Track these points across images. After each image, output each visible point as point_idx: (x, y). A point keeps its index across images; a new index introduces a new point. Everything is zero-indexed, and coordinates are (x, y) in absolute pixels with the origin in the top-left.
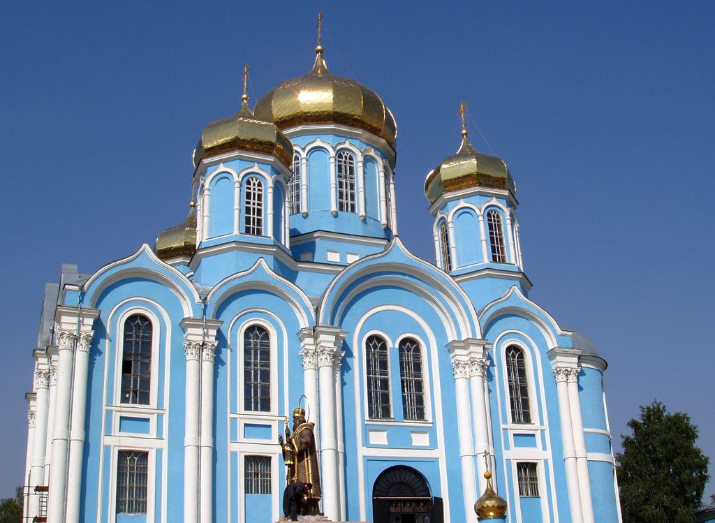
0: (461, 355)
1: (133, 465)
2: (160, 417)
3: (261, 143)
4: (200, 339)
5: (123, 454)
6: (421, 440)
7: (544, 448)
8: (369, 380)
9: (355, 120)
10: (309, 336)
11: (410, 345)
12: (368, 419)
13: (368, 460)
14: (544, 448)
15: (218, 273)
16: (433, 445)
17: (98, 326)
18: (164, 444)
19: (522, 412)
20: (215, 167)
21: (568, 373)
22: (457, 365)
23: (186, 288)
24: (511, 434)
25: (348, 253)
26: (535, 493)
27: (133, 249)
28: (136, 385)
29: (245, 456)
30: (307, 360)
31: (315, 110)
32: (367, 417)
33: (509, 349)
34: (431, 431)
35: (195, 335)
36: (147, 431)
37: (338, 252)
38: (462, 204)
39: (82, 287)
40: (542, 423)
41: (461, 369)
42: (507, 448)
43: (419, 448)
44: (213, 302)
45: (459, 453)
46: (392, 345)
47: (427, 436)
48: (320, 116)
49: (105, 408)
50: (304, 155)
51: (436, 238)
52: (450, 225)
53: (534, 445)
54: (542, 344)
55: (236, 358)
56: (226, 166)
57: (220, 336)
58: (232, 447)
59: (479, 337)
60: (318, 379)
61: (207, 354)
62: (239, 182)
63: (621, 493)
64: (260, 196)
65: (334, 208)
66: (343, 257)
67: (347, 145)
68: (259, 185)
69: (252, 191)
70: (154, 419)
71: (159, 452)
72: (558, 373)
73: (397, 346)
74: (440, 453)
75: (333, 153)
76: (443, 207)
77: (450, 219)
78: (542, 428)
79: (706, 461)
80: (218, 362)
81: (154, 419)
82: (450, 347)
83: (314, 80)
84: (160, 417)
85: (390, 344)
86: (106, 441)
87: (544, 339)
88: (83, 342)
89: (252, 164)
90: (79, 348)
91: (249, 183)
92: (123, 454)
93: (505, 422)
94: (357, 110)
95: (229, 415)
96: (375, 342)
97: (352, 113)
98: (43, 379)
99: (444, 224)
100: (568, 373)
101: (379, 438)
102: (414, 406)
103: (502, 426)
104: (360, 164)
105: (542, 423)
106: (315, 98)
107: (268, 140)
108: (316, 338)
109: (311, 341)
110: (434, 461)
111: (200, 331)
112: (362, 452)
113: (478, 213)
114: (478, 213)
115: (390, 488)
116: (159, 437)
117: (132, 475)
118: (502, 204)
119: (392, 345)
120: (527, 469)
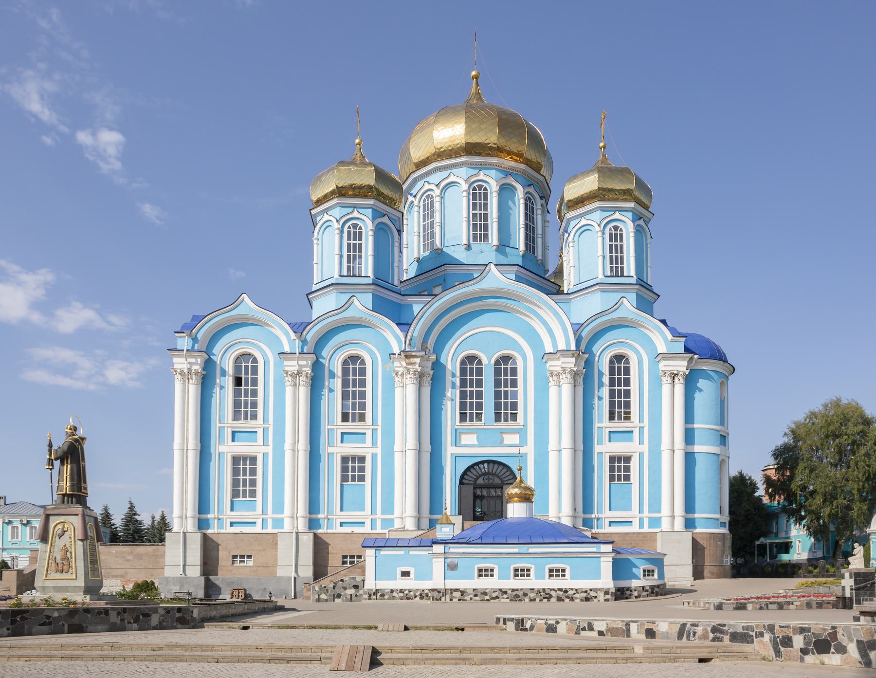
0: (556, 365)
2: (265, 430)
3: (361, 187)
4: (295, 369)
5: (345, 459)
7: (641, 442)
9: (491, 148)
13: (456, 457)
14: (641, 442)
15: (587, 307)
16: (523, 442)
17: (209, 364)
18: (269, 450)
21: (674, 376)
27: (235, 302)
28: (620, 409)
30: (396, 379)
31: (447, 145)
32: (458, 423)
34: (522, 432)
43: (506, 445)
46: (488, 362)
48: (453, 149)
50: (437, 192)
53: (631, 440)
58: (222, 449)
59: (573, 348)
61: (303, 381)
62: (338, 229)
63: (171, 466)
67: (481, 176)
70: (260, 432)
73: (493, 362)
74: (529, 449)
75: (465, 186)
78: (641, 425)
81: (260, 432)
82: (545, 356)
83: (445, 112)
84: (265, 430)
85: (485, 361)
86: (222, 449)
92: (345, 459)
94: (492, 138)
97: (487, 142)
102: (505, 410)
106: (451, 132)
107: (367, 183)
112: (449, 450)
115: (480, 476)
116: (265, 444)
119: (488, 362)
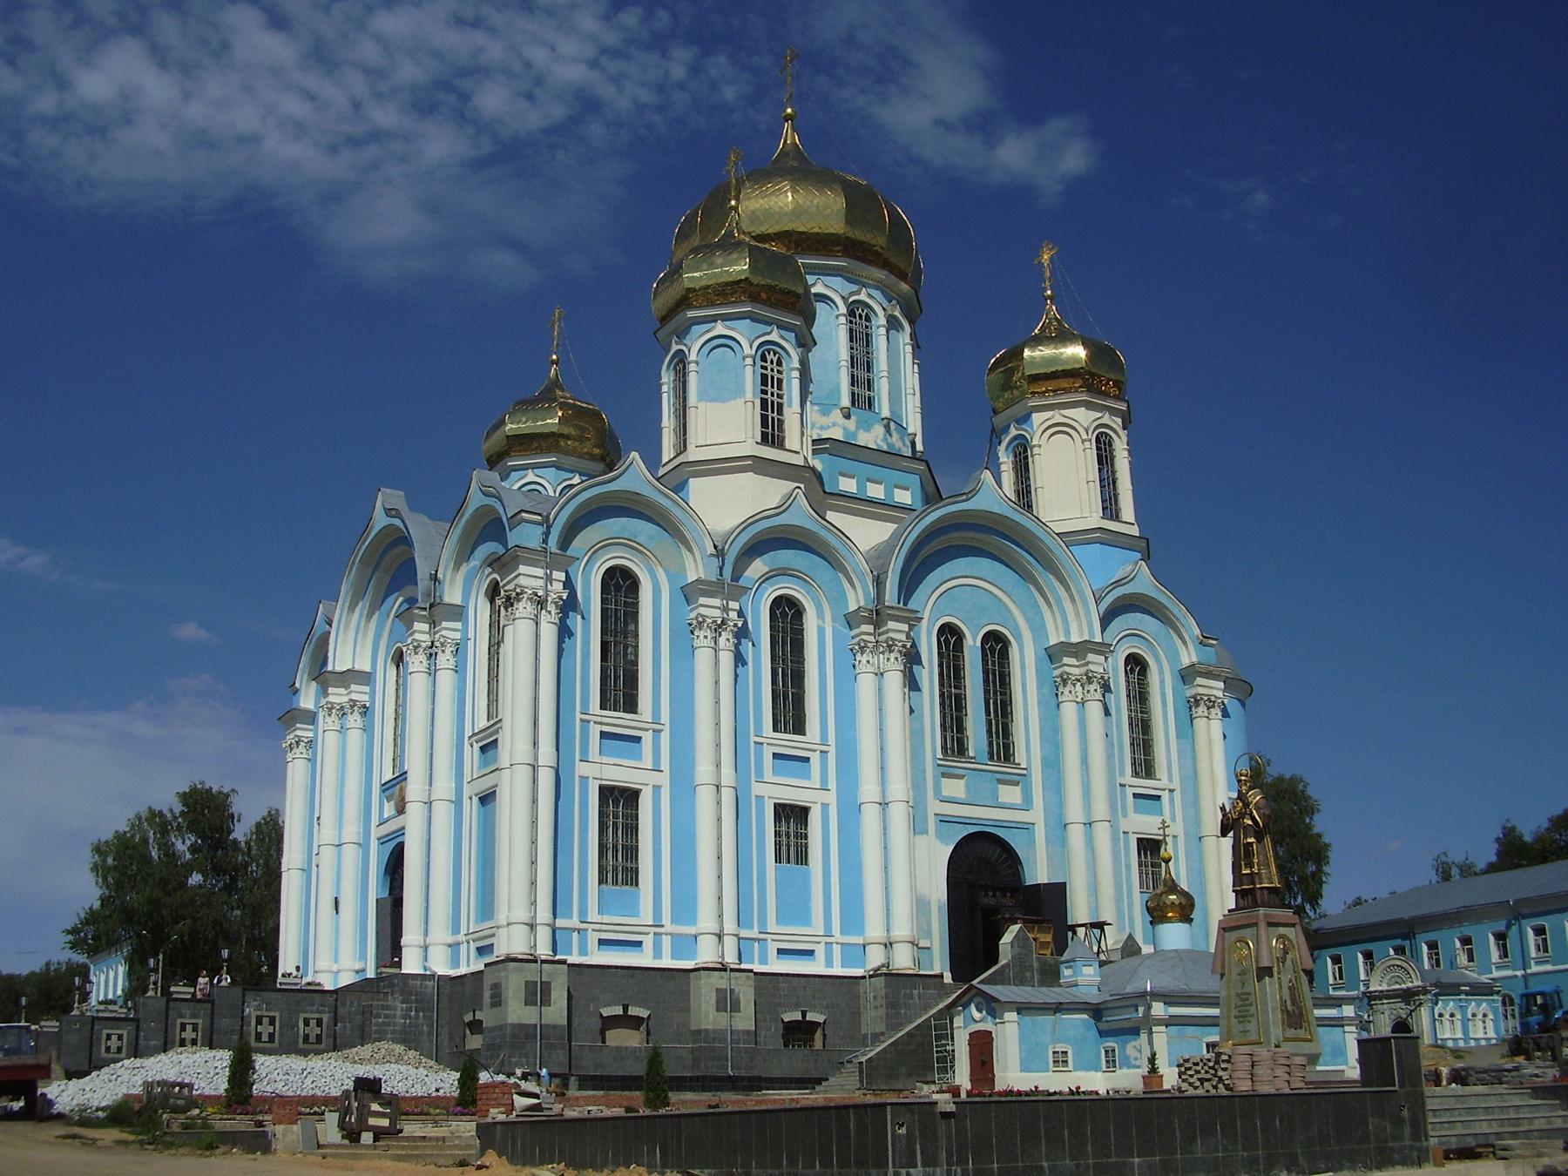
1: (620, 803)
6: (1009, 794)
8: (942, 695)
10: (869, 621)
11: (996, 646)
12: (598, 711)
16: (1027, 805)
19: (620, 688)
20: (708, 326)
22: (700, 623)
23: (1085, 604)
24: (768, 752)
25: (897, 487)
26: (802, 857)
29: (601, 787)
33: (611, 572)
35: (710, 608)
36: (638, 756)
37: (879, 483)
38: (720, 329)
39: (548, 517)
40: (1170, 780)
41: (1069, 687)
42: (1125, 816)
44: (732, 554)
45: (692, 777)
47: (1018, 789)
49: (578, 716)
51: (665, 388)
52: (692, 367)
54: (1173, 657)
55: (929, 674)
56: (727, 327)
57: (568, 584)
60: (537, 636)
64: (780, 381)
65: (846, 401)
66: (861, 487)
67: (863, 297)
68: (779, 363)
69: (769, 372)
71: (825, 806)
72: (1197, 703)
74: (1036, 815)
75: (843, 309)
76: (682, 333)
77: (693, 357)
79: (1327, 846)
80: (564, 632)
87: (1175, 650)
88: (552, 608)
89: (769, 329)
90: (722, 640)
91: (764, 359)
93: (1122, 774)
95: (754, 739)
96: (950, 637)
98: (422, 657)
99: (681, 361)
100: (720, 627)
101: (954, 788)
103: (754, 739)
104: (883, 331)
105: (1170, 780)
108: (877, 626)
109: (870, 628)
110: (1027, 827)
111: (717, 602)
113: (747, 350)
114: (747, 350)
117: (615, 825)
118: (1117, 422)
120: (792, 816)
